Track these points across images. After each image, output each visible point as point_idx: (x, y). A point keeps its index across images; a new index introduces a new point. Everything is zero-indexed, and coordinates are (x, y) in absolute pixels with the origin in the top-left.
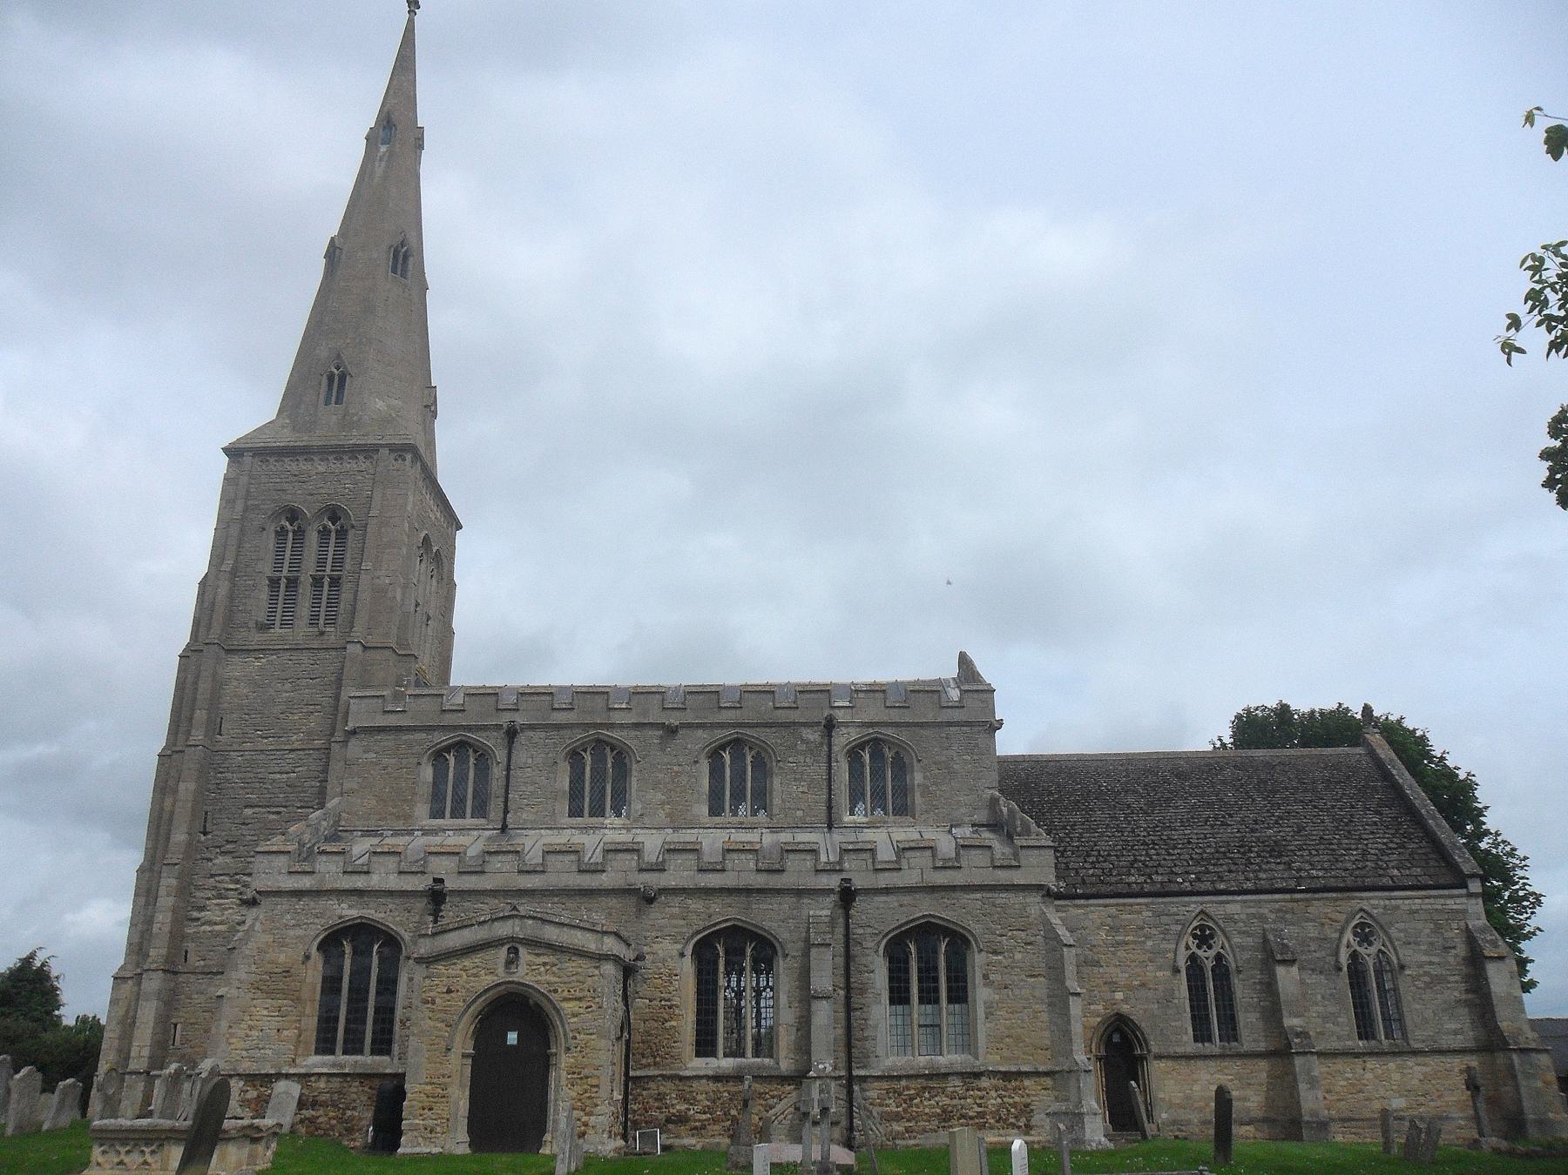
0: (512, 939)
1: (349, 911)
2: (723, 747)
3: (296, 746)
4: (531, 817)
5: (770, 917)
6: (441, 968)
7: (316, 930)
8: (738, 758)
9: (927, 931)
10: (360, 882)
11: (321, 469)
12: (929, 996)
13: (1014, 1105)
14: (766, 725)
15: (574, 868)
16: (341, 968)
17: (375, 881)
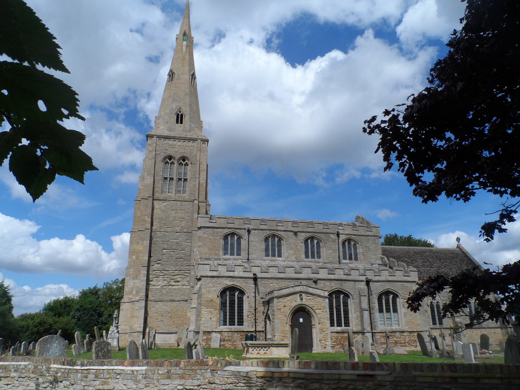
0: (301, 292)
1: (229, 283)
2: (308, 239)
3: (178, 231)
4: (256, 256)
5: (347, 287)
6: (281, 300)
7: (220, 288)
8: (312, 242)
9: (387, 293)
10: (231, 274)
11: (179, 144)
12: (388, 311)
13: (413, 340)
14: (320, 233)
15: (293, 272)
16: (226, 300)
17: (236, 274)
